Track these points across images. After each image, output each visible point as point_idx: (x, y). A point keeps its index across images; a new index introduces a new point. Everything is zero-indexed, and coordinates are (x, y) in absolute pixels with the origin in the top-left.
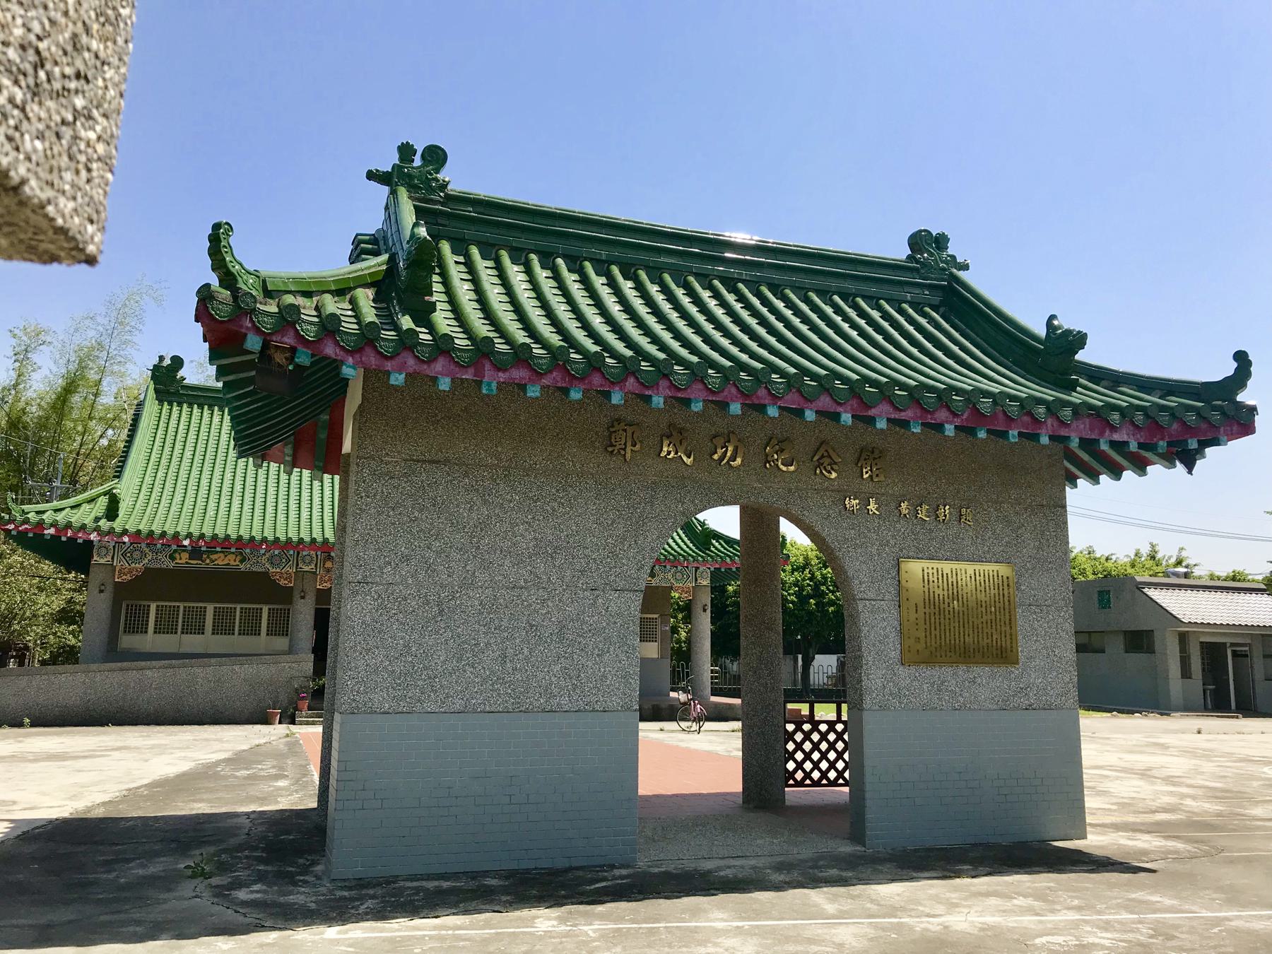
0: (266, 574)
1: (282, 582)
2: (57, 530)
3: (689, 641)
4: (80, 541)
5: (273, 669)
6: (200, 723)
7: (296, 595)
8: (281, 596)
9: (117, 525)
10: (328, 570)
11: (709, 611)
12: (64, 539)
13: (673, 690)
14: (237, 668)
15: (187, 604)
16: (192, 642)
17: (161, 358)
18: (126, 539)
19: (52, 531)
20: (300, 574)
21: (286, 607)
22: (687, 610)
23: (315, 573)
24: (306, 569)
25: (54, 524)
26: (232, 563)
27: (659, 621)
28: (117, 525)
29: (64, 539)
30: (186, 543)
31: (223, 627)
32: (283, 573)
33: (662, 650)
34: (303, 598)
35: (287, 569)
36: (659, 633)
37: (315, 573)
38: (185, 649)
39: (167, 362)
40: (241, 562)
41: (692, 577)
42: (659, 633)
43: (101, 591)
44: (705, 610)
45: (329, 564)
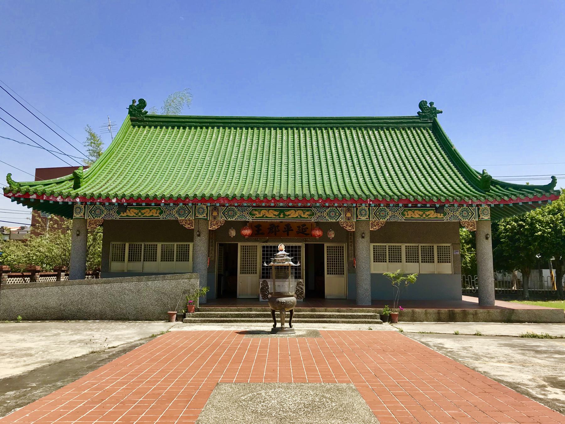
0: (177, 221)
1: (187, 226)
2: (37, 196)
3: (474, 261)
4: (51, 202)
5: (174, 283)
6: (136, 319)
7: (196, 234)
8: (181, 234)
9: (80, 191)
10: (215, 218)
11: (490, 239)
12: (42, 201)
13: (466, 293)
14: (150, 283)
15: (146, 243)
16: (150, 266)
17: (134, 101)
18: (78, 200)
19: (34, 196)
20: (197, 220)
21: (388, 260)
22: (473, 241)
23: (206, 219)
24: (201, 217)
25: (35, 193)
26: (154, 215)
27: (451, 248)
28: (80, 191)
29: (42, 201)
30: (114, 201)
31: (167, 256)
32: (186, 220)
33: (455, 268)
34: (199, 235)
35: (189, 217)
36: (452, 257)
37: (206, 219)
38: (146, 270)
39: (137, 103)
40: (160, 214)
41: (475, 214)
42: (452, 257)
43: (78, 235)
44: (487, 238)
45: (215, 214)
